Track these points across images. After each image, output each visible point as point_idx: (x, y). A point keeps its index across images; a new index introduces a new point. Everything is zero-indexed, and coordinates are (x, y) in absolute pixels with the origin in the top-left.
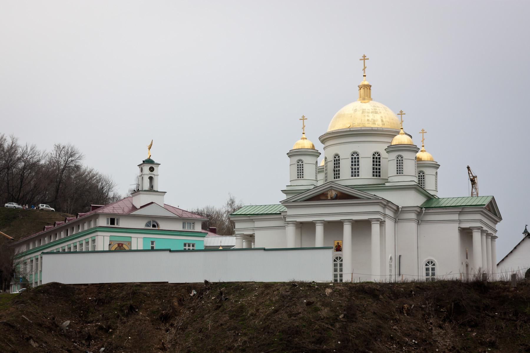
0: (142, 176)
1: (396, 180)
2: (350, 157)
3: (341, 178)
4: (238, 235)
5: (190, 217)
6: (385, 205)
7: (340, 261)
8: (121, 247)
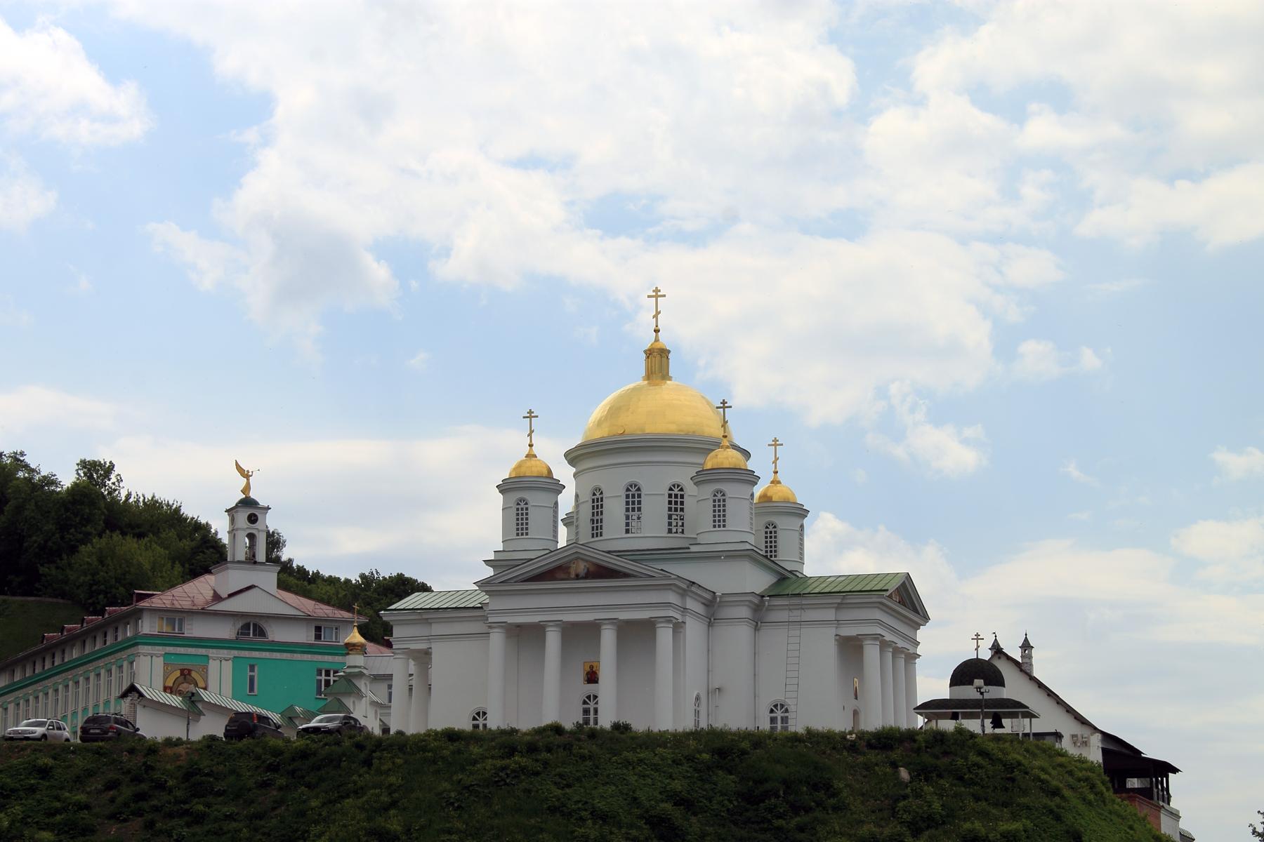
0: (234, 532)
1: (712, 538)
2: (667, 492)
3: (604, 537)
4: (397, 651)
5: (331, 616)
6: (684, 590)
7: (782, 712)
8: (188, 676)
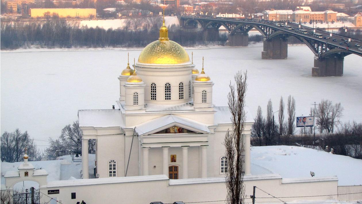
2: (178, 85)
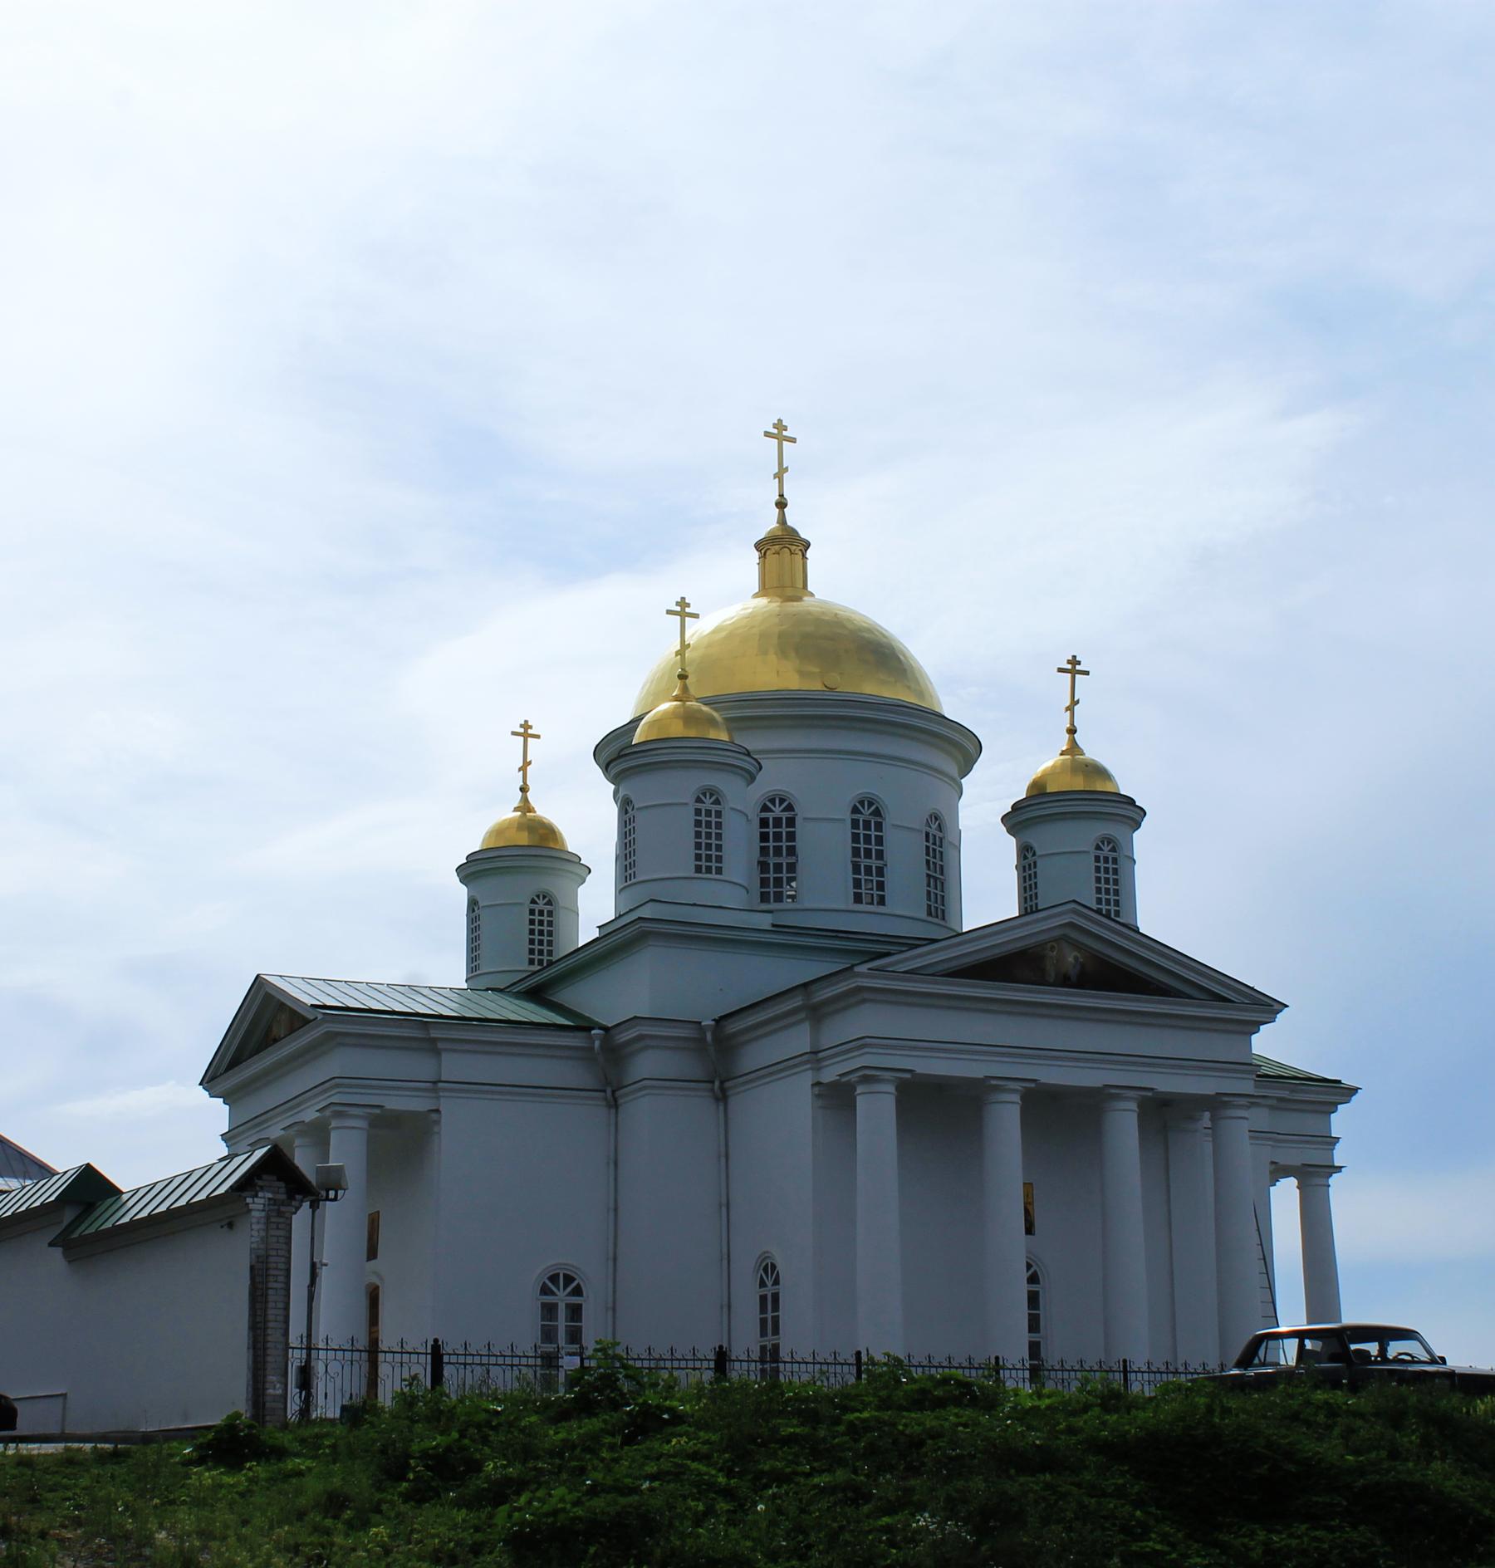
2: (848, 816)
